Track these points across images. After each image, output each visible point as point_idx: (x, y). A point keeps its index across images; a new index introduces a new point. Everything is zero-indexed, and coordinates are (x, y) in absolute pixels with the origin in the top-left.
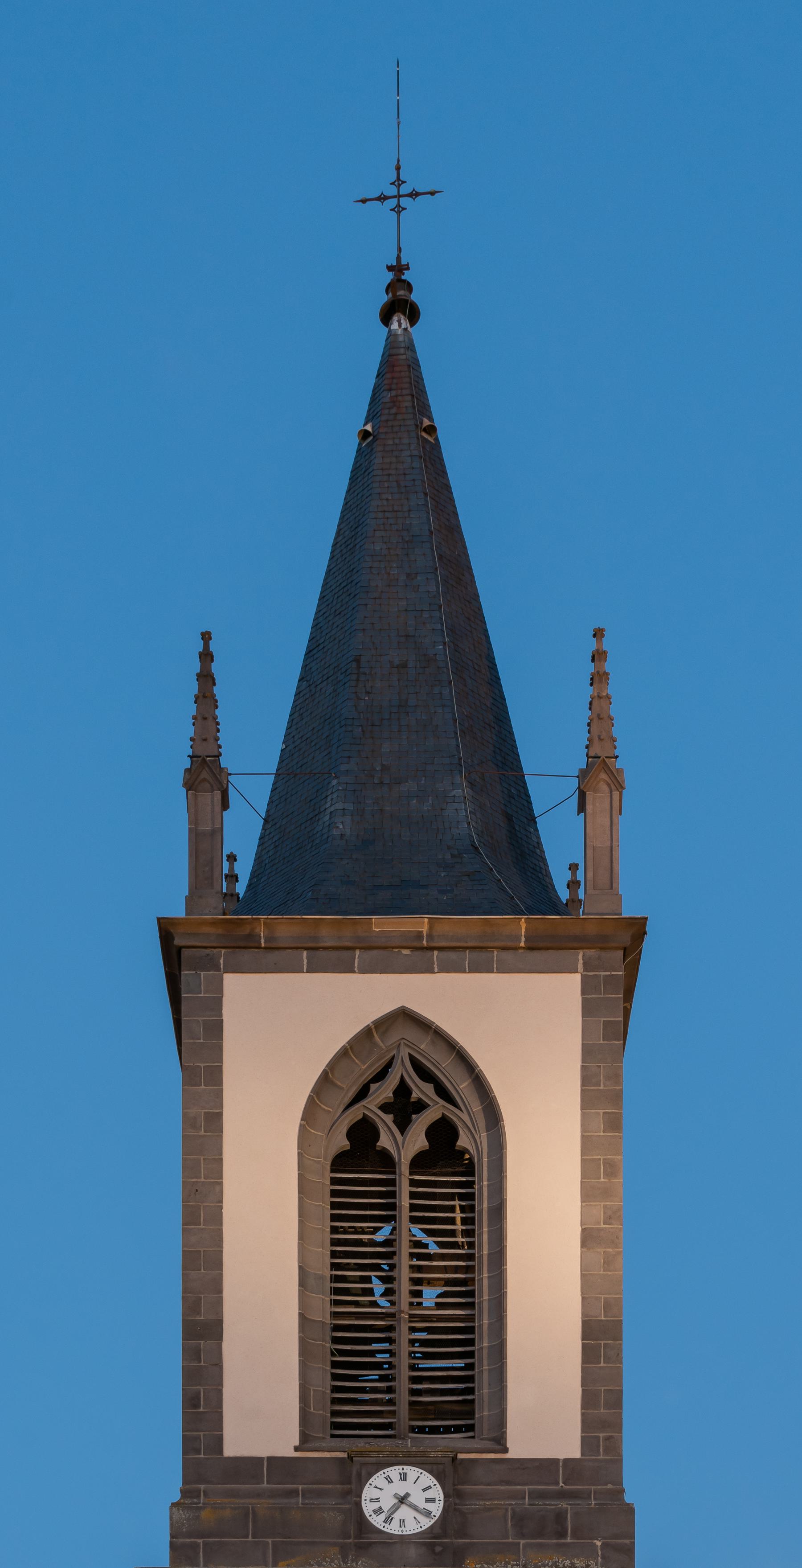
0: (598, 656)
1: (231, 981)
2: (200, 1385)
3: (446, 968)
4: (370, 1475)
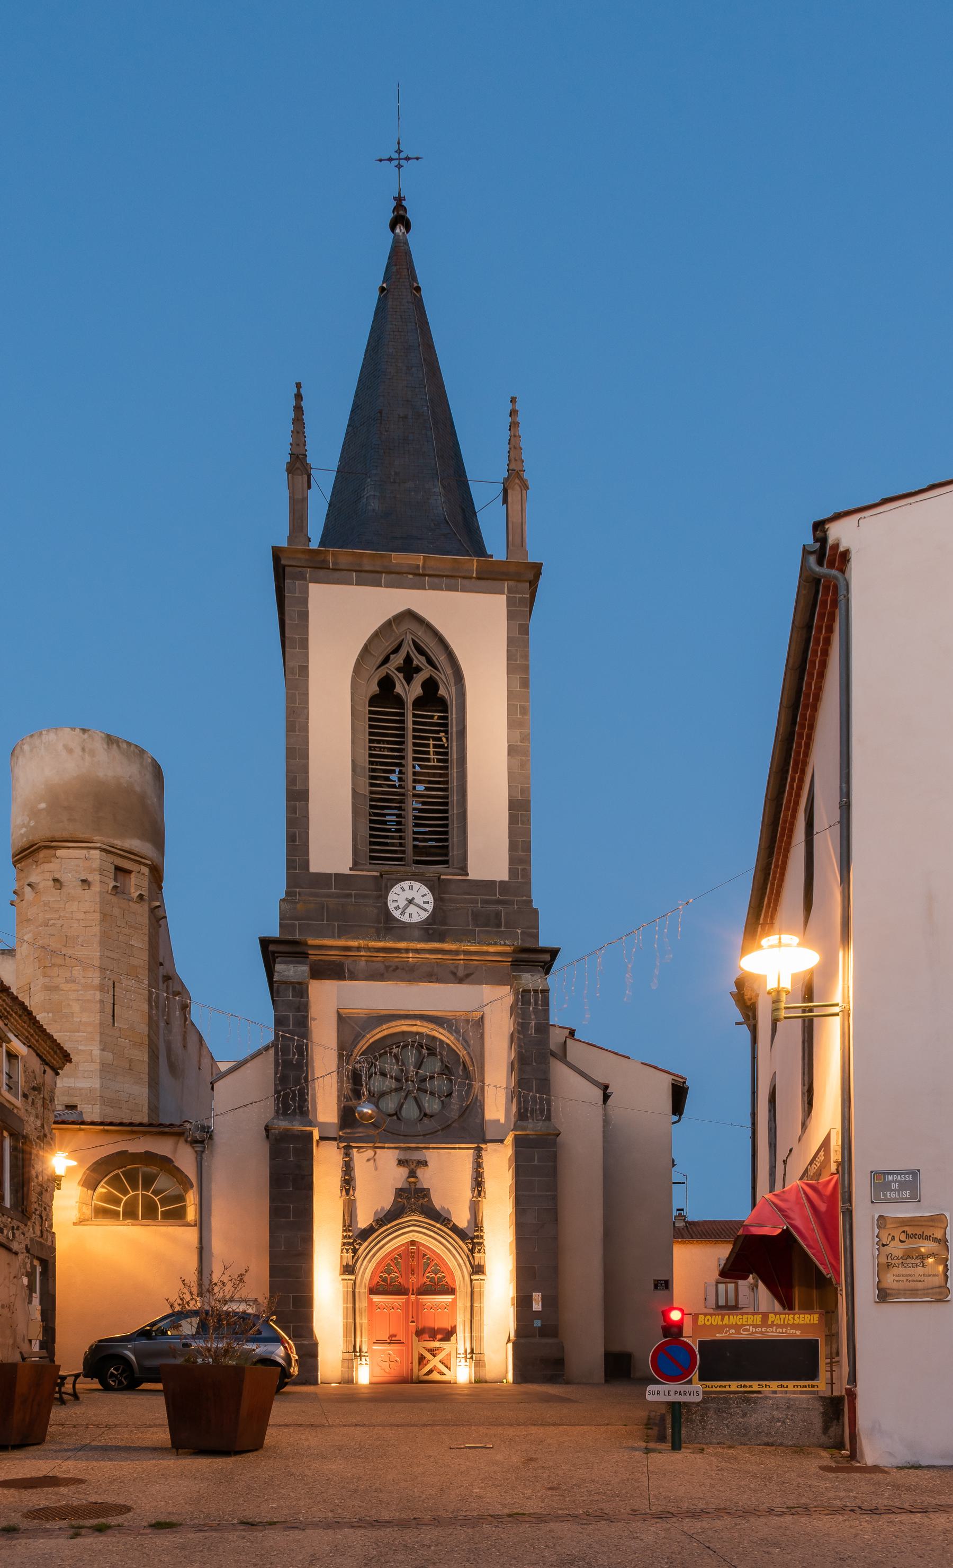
0: (513, 413)
1: (313, 588)
3: (433, 587)
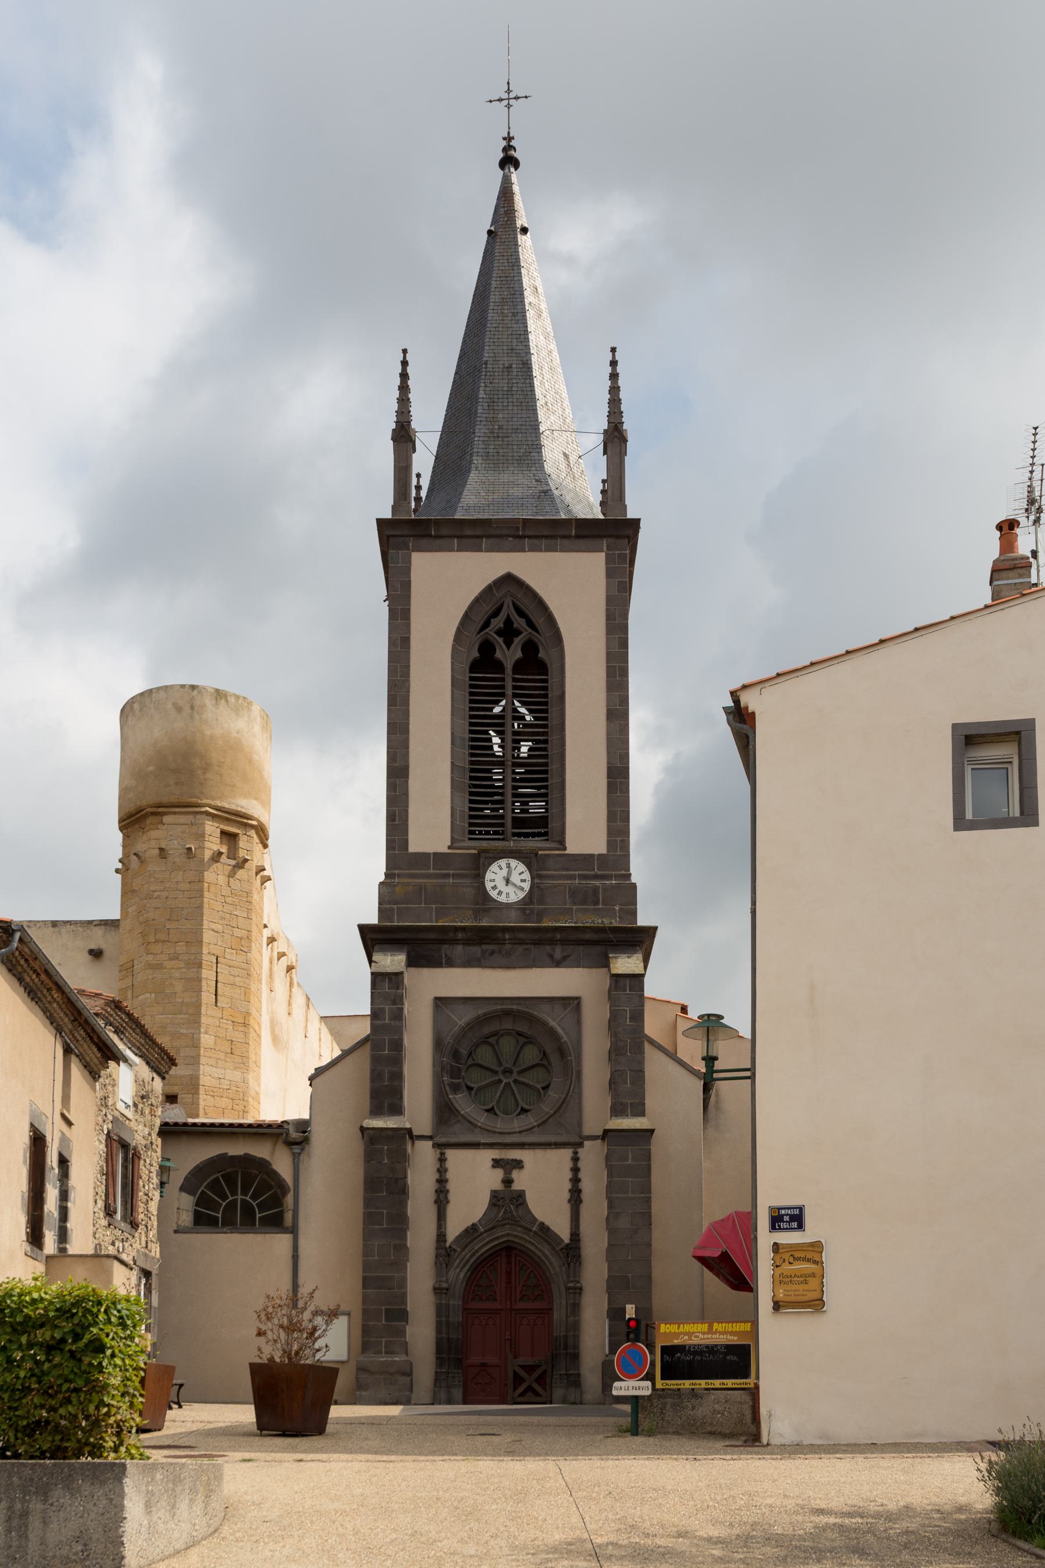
4: (490, 865)
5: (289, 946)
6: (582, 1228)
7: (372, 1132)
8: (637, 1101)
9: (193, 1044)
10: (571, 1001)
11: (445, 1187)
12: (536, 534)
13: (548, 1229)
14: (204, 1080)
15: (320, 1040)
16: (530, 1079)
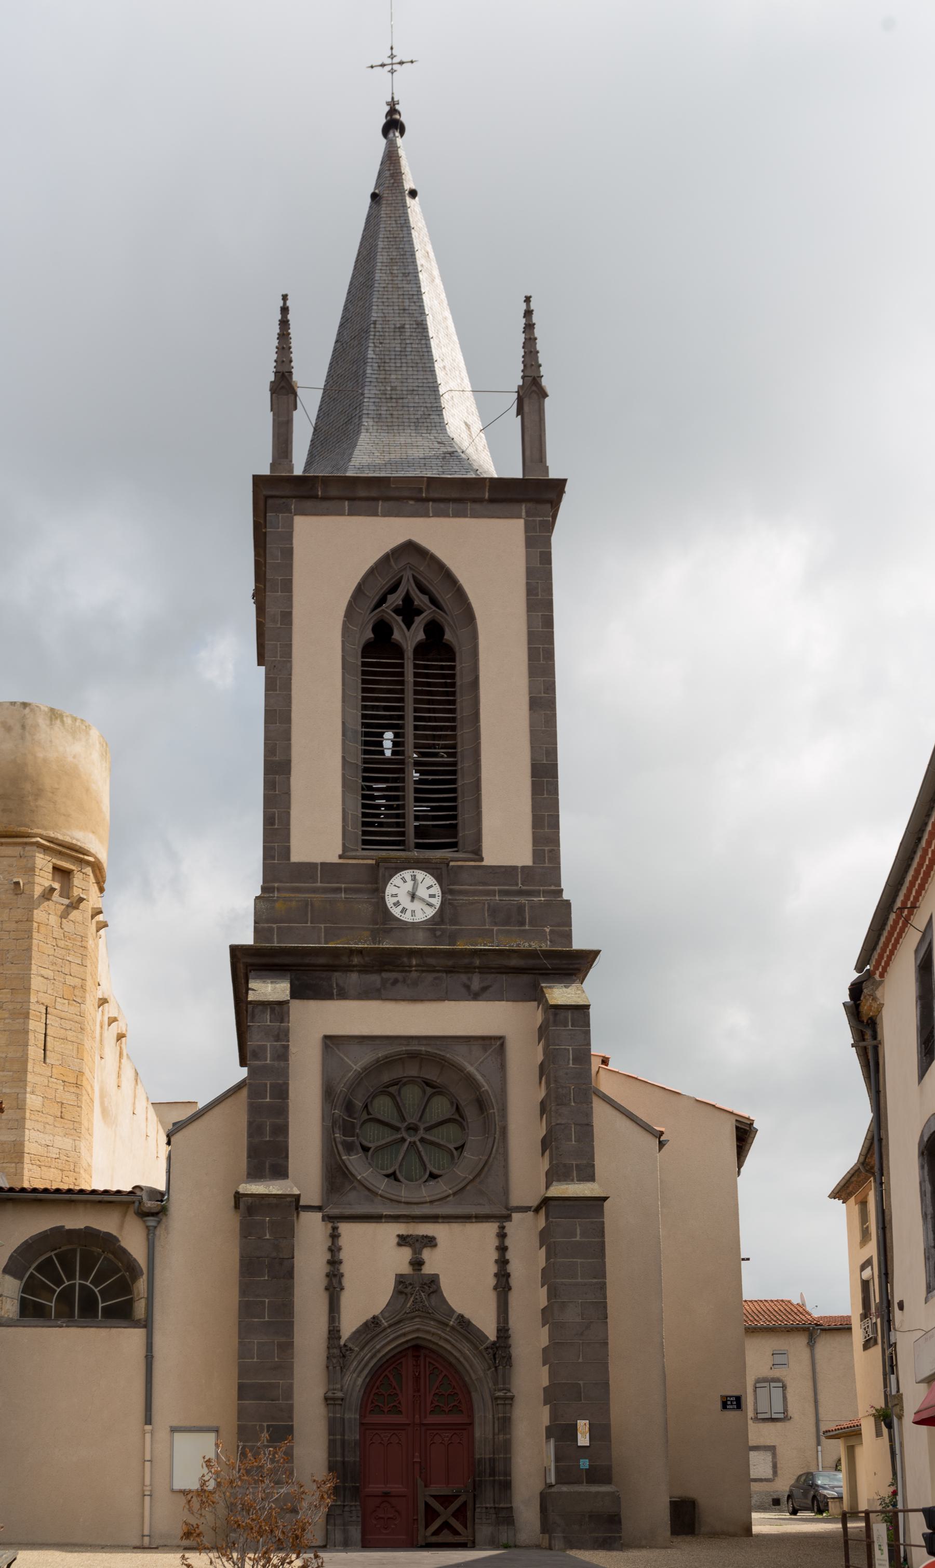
2: (275, 808)
4: (391, 876)
5: (119, 1012)
6: (512, 1323)
7: (250, 1200)
8: (585, 1162)
9: (18, 1104)
10: (493, 1041)
11: (338, 1270)
12: (443, 496)
13: (469, 1323)
14: (30, 1147)
15: (147, 1119)
16: (438, 1138)
